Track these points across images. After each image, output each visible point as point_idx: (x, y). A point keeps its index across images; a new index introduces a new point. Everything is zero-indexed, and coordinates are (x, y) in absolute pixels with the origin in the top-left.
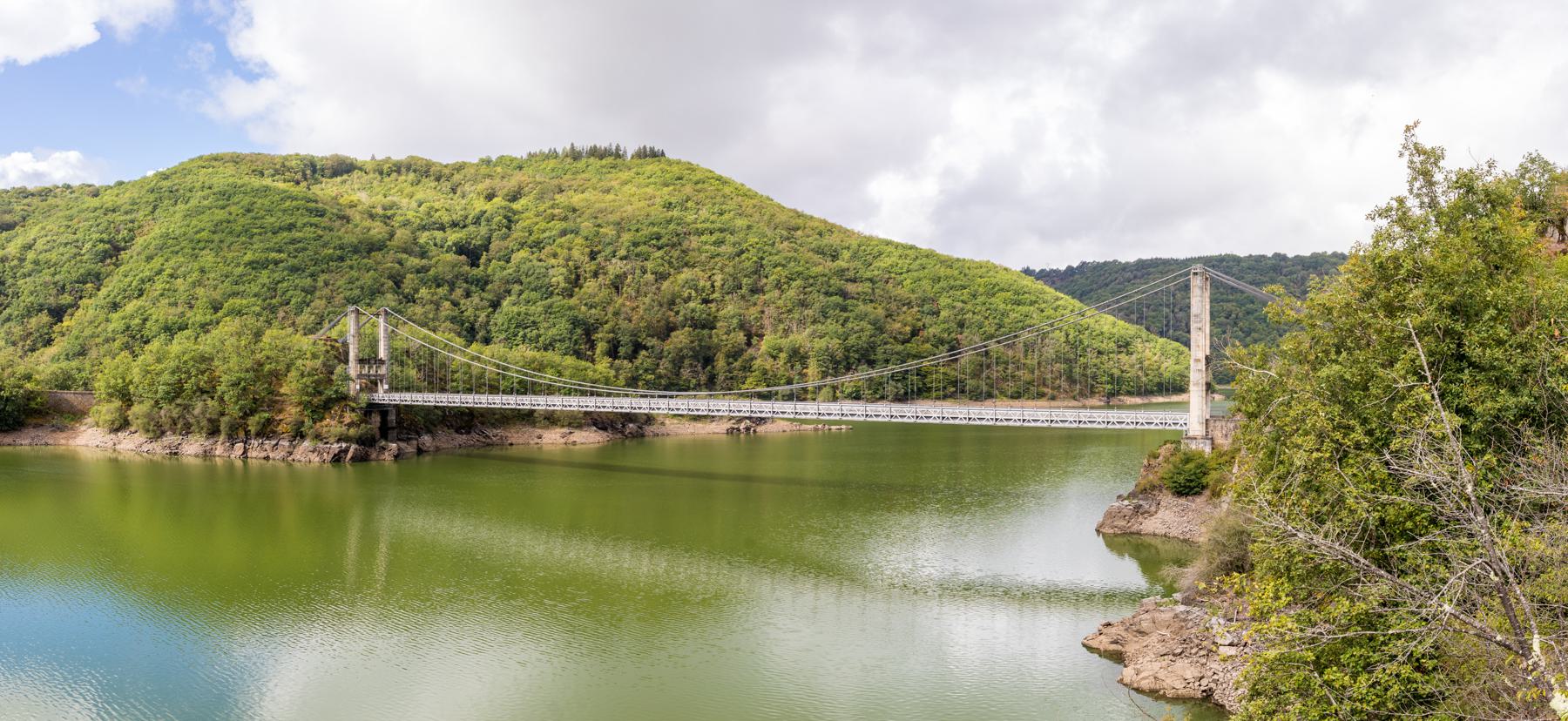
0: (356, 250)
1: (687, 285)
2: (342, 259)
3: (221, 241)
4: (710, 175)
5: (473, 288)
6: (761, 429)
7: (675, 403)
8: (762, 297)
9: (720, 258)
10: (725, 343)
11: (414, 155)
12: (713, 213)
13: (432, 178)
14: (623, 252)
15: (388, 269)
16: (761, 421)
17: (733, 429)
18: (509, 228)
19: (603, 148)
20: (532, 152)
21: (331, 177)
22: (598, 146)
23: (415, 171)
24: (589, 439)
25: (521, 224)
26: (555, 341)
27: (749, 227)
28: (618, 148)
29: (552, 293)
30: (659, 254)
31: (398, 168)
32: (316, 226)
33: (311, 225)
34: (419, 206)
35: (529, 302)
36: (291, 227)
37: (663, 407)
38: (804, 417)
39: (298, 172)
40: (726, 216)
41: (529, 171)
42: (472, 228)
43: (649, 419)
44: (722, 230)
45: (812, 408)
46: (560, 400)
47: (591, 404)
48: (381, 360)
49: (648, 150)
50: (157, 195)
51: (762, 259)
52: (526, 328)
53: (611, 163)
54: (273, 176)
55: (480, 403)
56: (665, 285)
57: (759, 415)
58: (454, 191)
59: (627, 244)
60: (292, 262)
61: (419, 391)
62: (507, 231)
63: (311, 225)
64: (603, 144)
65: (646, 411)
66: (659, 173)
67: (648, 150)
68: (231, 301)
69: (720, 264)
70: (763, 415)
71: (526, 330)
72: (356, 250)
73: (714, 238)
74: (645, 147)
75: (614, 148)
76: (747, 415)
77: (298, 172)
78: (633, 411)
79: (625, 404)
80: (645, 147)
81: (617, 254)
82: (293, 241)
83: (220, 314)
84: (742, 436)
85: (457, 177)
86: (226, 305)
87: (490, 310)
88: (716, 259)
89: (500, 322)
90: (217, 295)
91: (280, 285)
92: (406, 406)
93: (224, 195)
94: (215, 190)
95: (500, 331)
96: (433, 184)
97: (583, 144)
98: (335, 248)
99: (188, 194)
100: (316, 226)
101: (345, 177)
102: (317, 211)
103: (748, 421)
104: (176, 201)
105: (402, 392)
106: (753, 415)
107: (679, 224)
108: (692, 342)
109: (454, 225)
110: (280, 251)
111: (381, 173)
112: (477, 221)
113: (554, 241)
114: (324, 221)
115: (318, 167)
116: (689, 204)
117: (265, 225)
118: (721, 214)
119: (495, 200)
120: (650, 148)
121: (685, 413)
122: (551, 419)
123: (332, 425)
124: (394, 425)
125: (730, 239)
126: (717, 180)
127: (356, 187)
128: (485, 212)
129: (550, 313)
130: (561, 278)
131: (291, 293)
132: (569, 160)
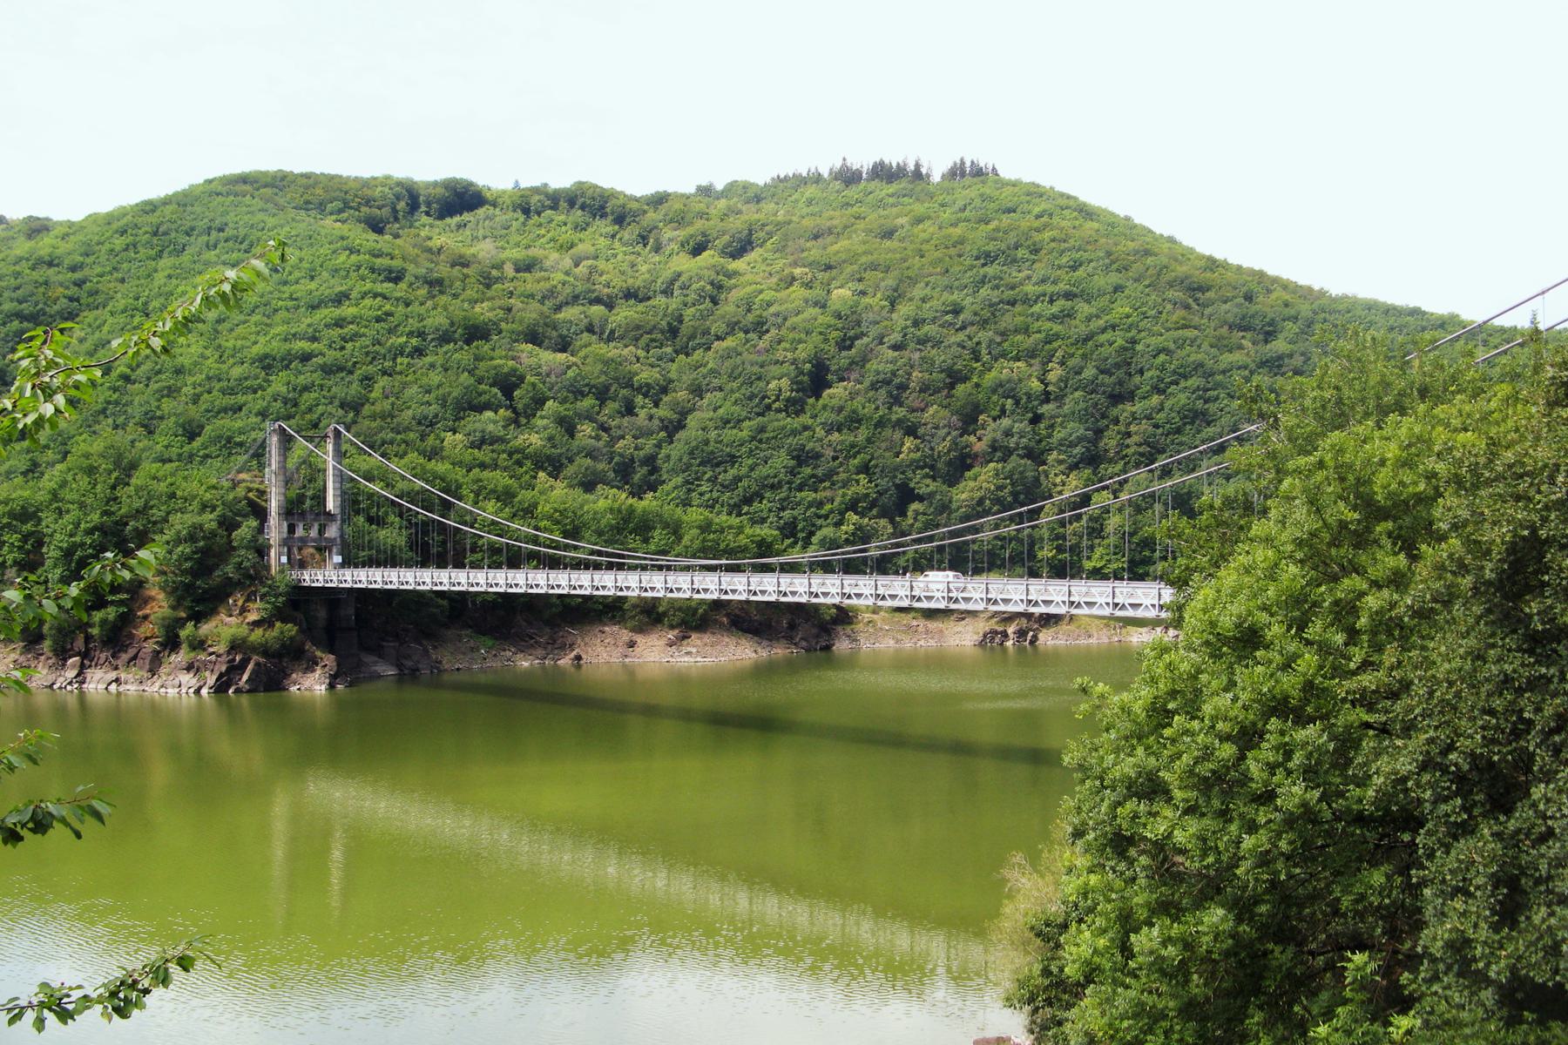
0: (445, 338)
1: (1001, 391)
2: (419, 352)
3: (219, 321)
4: (1063, 202)
5: (639, 400)
6: (1047, 638)
7: (1084, 589)
8: (1129, 407)
9: (1060, 342)
10: (1060, 488)
11: (584, 180)
12: (1060, 267)
13: (610, 218)
14: (896, 337)
15: (495, 368)
16: (1048, 620)
17: (996, 633)
18: (715, 302)
19: (894, 165)
20: (782, 176)
21: (441, 217)
22: (887, 162)
23: (583, 208)
24: (739, 653)
25: (735, 295)
26: (764, 486)
27: (1118, 289)
28: (918, 166)
29: (769, 407)
30: (961, 336)
31: (556, 200)
32: (385, 297)
33: (375, 296)
34: (577, 265)
35: (728, 422)
36: (340, 299)
37: (1058, 599)
38: (1130, 613)
39: (383, 206)
40: (1081, 272)
41: (768, 207)
42: (660, 301)
43: (843, 616)
44: (1069, 296)
45: (1101, 594)
46: (838, 582)
47: (740, 587)
48: (329, 514)
49: (968, 164)
50: (130, 239)
51: (1134, 342)
52: (718, 465)
53: (904, 189)
54: (340, 211)
55: (929, 598)
56: (961, 389)
57: (1043, 609)
58: (643, 239)
59: (901, 323)
60: (331, 356)
61: (408, 564)
62: (711, 305)
63: (375, 296)
64: (893, 159)
65: (837, 600)
66: (978, 202)
67: (968, 164)
68: (219, 423)
69: (1059, 354)
70: (1052, 610)
71: (717, 470)
72: (445, 338)
73: (1055, 309)
74: (962, 160)
75: (911, 167)
76: (1021, 608)
77: (383, 206)
78: (814, 600)
79: (798, 588)
80: (962, 160)
81: (886, 340)
82: (339, 323)
83: (197, 443)
84: (1009, 644)
85: (651, 216)
86: (208, 428)
87: (663, 434)
88: (1055, 345)
89: (675, 454)
90: (194, 412)
91: (306, 396)
92: (560, 596)
93: (241, 243)
94: (229, 232)
95: (673, 471)
96: (610, 229)
97: (863, 160)
98: (410, 334)
99: (183, 239)
100: (385, 297)
101: (466, 216)
102: (390, 272)
103: (1024, 621)
104: (161, 251)
105: (371, 567)
106: (1032, 610)
107: (997, 287)
108: (1000, 488)
109: (630, 295)
110: (314, 339)
111: (526, 211)
112: (667, 292)
113: (785, 319)
114: (401, 290)
115: (421, 198)
116: (1020, 253)
117: (299, 295)
118: (1074, 268)
119: (706, 254)
120: (972, 162)
121: (981, 606)
122: (650, 615)
123: (225, 627)
124: (353, 624)
125: (1084, 309)
126: (1075, 210)
127: (481, 233)
128: (679, 275)
129: (760, 441)
130: (785, 383)
131: (321, 409)
132: (838, 185)
